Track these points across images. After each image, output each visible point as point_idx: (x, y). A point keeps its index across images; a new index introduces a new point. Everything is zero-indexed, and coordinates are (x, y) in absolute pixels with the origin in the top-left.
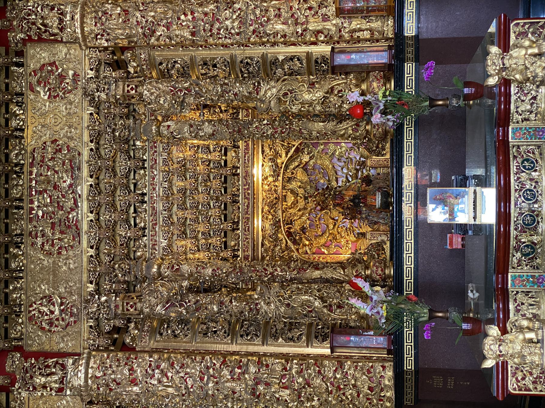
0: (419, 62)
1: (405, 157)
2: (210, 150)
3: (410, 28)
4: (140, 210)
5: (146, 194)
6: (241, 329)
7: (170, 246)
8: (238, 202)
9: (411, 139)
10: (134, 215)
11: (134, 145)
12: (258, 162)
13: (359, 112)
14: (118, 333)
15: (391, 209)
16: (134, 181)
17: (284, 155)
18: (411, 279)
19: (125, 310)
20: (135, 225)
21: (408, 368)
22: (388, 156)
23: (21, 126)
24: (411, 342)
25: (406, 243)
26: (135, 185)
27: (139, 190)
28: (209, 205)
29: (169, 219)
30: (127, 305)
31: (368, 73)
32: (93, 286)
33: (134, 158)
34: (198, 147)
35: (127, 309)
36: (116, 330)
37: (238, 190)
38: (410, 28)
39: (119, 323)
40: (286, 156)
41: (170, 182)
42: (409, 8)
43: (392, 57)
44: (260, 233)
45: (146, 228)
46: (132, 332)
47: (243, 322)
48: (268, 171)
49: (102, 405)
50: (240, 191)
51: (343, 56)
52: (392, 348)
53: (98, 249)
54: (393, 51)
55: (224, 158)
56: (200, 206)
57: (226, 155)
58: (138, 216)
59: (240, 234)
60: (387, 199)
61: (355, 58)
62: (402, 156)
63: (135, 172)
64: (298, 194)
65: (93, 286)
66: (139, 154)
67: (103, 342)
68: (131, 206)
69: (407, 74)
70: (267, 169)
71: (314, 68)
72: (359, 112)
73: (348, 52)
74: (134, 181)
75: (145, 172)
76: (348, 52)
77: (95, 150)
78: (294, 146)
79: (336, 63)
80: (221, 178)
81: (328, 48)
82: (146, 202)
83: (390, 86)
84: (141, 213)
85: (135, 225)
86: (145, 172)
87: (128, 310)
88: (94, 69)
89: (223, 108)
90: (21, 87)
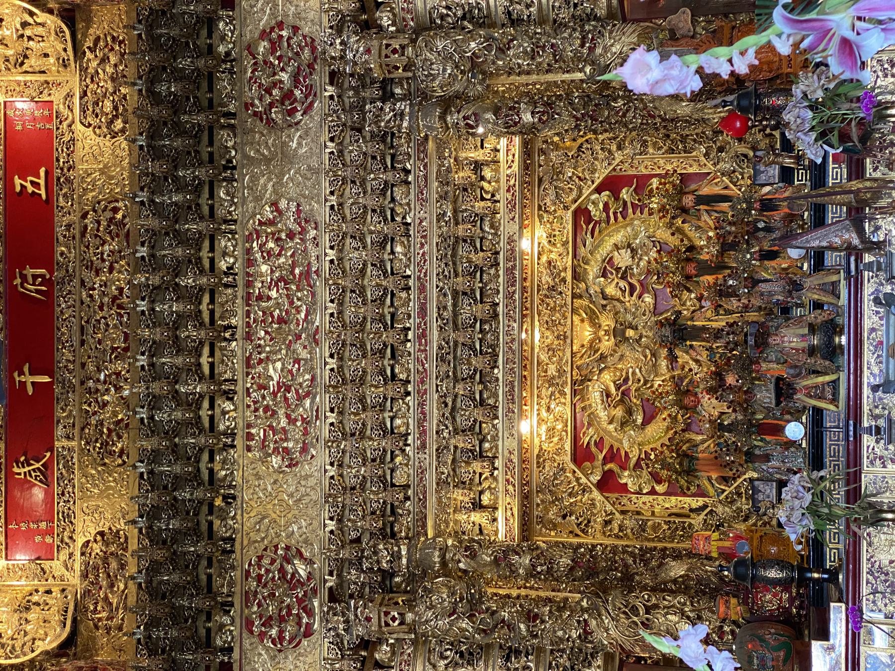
4: (400, 511)
5: (409, 329)
19: (383, 624)
23: (233, 429)
26: (393, 315)
30: (386, 48)
32: (334, 415)
33: (392, 273)
35: (386, 622)
45: (409, 434)
49: (350, 660)
58: (397, 362)
63: (393, 295)
64: (600, 326)
65: (335, 361)
68: (387, 347)
75: (409, 295)
77: (336, 263)
84: (401, 515)
87: (387, 625)
90: (233, 370)
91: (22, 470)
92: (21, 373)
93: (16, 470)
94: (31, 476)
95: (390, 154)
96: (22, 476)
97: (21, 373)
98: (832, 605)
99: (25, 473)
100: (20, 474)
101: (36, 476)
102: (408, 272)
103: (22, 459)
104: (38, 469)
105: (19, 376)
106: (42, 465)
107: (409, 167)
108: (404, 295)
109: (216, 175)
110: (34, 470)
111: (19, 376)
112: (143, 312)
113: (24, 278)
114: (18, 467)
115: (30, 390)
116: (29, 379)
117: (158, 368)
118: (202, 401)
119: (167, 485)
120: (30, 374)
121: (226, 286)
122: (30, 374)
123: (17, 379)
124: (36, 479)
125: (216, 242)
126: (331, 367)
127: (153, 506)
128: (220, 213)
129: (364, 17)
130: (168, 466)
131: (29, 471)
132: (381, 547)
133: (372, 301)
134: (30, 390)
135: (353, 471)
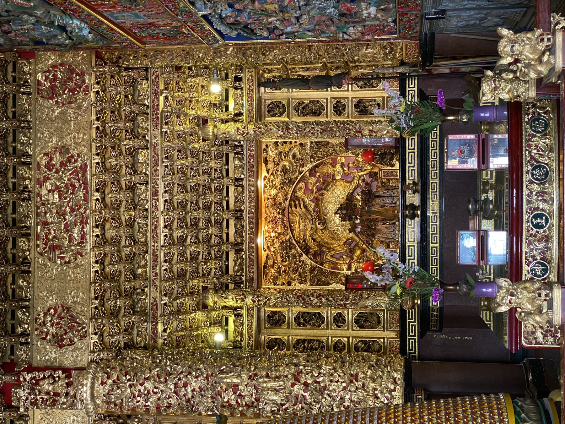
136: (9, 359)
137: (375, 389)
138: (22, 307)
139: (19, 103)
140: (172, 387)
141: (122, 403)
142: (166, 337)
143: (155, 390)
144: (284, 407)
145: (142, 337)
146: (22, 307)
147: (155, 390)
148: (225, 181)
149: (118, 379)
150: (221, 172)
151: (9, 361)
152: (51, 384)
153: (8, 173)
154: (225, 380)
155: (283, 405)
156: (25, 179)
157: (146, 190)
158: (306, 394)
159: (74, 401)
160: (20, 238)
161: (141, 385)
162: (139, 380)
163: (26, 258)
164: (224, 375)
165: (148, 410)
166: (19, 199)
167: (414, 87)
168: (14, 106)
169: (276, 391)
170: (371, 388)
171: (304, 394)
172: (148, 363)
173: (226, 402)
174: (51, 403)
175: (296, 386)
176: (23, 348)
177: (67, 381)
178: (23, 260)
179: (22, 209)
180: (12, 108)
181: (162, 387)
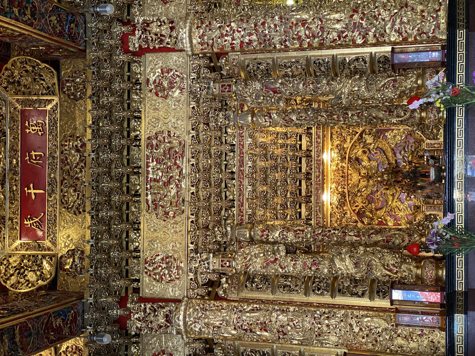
0: (469, 29)
1: (457, 121)
2: (287, 136)
3: (460, 329)
6: (313, 285)
7: (254, 191)
8: (311, 179)
9: (463, 72)
10: (225, 190)
11: (226, 132)
12: (328, 149)
13: (415, 249)
14: (211, 286)
15: (443, 182)
16: (225, 162)
17: (349, 141)
18: (462, 280)
20: (226, 197)
21: (462, 31)
22: (442, 139)
24: (462, 268)
25: (459, 54)
27: (229, 169)
28: (287, 182)
29: (253, 216)
31: (424, 69)
32: (193, 245)
34: (278, 134)
35: (225, 85)
36: (211, 283)
37: (312, 169)
38: (460, 329)
39: (214, 277)
40: (351, 142)
41: (254, 162)
42: (459, 157)
43: (446, 55)
44: (329, 207)
46: (224, 286)
47: (314, 279)
48: (335, 155)
50: (313, 170)
51: (402, 56)
52: (446, 60)
53: (197, 216)
54: (446, 51)
55: (299, 142)
56: (279, 160)
57: (301, 140)
59: (313, 206)
60: (440, 173)
61: (412, 58)
62: (454, 148)
63: (226, 154)
66: (229, 139)
67: (202, 291)
69: (459, 38)
70: (335, 198)
71: (377, 65)
72: (415, 249)
73: (407, 52)
74: (225, 162)
75: (234, 154)
76: (407, 52)
78: (357, 133)
79: (396, 61)
80: (297, 136)
81: (389, 48)
82: (234, 179)
83: (442, 273)
85: (226, 197)
86: (234, 154)
88: (195, 186)
89: (298, 102)
91: (28, 222)
92: (29, 188)
93: (26, 222)
94: (34, 226)
95: (223, 247)
96: (29, 226)
97: (29, 188)
98: (456, 315)
99: (31, 224)
100: (27, 225)
101: (36, 225)
102: (234, 143)
103: (29, 216)
104: (37, 221)
105: (28, 190)
106: (39, 220)
107: (234, 171)
108: (232, 154)
109: (132, 88)
110: (35, 222)
111: (28, 190)
112: (91, 303)
113: (31, 157)
114: (27, 221)
115: (33, 197)
116: (32, 191)
117: (100, 188)
118: (123, 206)
119: (105, 307)
120: (34, 189)
121: (134, 258)
122: (34, 189)
123: (27, 191)
124: (36, 227)
125: (131, 122)
126: (192, 163)
127: (96, 348)
128: (131, 218)
129: (212, 64)
130: (105, 298)
131: (33, 223)
132: (216, 229)
133: (214, 214)
134: (33, 197)
135: (205, 219)
136: (127, 19)
137: (423, 11)
138: (134, 343)
139: (132, 153)
140: (253, 25)
141: (213, 43)
142: (250, 213)
143: (239, 29)
144: (344, 35)
145: (230, 192)
146: (134, 343)
147: (239, 29)
148: (298, 176)
149: (210, 23)
150: (296, 146)
151: (126, 21)
152: (159, 26)
153: (123, 151)
154: (295, 17)
155: (343, 32)
156: (137, 74)
157: (234, 158)
158: (363, 22)
159: (176, 41)
160: (133, 175)
161: (228, 26)
162: (226, 23)
163: (138, 80)
164: (294, 13)
165: (233, 48)
166: (130, 257)
167: (463, 51)
168: (128, 154)
169: (338, 21)
170: (419, 11)
171: (361, 21)
172: (233, 12)
173: (295, 35)
174: (159, 42)
175: (354, 16)
176: (136, 148)
177: (170, 25)
178: (135, 192)
179: (133, 178)
180: (127, 72)
181: (245, 25)
